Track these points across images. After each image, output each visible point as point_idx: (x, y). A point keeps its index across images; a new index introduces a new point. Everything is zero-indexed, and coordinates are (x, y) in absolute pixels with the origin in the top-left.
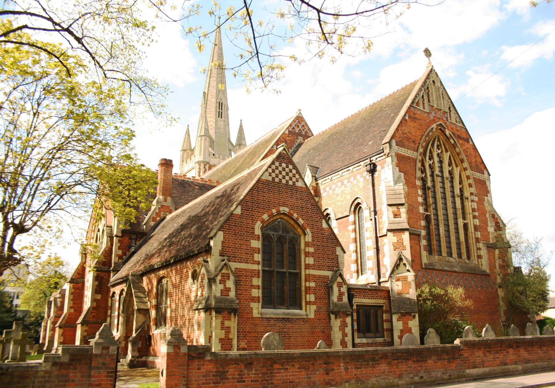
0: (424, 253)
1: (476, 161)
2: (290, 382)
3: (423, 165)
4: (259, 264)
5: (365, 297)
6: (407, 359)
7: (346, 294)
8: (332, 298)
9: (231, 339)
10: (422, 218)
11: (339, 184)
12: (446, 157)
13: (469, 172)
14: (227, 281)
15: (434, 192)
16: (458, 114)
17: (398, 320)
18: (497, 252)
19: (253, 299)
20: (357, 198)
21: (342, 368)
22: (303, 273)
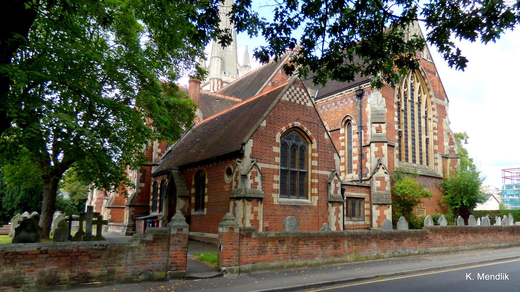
0: (396, 160)
1: (439, 91)
2: (310, 254)
3: (399, 92)
4: (278, 165)
5: (352, 191)
6: (390, 239)
7: (340, 189)
8: (330, 191)
9: (258, 221)
10: (396, 133)
11: (334, 104)
12: (417, 85)
13: (433, 99)
14: (256, 177)
15: (406, 114)
16: (429, 52)
17: (377, 209)
18: (449, 161)
19: (274, 191)
20: (347, 116)
21: (346, 245)
22: (310, 172)
